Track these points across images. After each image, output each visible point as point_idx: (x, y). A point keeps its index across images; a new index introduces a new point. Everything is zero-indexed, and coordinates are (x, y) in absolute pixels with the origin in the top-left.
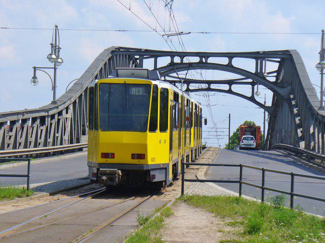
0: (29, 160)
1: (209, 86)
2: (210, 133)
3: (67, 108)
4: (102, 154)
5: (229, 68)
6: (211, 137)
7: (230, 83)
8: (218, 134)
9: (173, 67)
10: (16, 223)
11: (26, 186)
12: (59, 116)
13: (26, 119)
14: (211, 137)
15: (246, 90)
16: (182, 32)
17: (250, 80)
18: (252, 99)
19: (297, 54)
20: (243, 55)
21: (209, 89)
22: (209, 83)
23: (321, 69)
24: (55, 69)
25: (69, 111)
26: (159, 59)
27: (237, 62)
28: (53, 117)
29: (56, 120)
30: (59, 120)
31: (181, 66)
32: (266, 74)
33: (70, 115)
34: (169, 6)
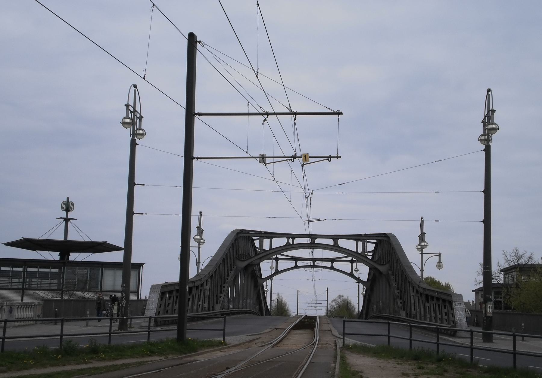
0: (225, 318)
1: (314, 263)
2: (310, 305)
3: (207, 281)
4: (472, 290)
5: (336, 247)
6: (311, 308)
7: (333, 260)
8: (318, 305)
9: (289, 247)
10: (241, 361)
11: (222, 339)
12: (201, 287)
13: (165, 292)
14: (311, 308)
15: (346, 267)
16: (320, 219)
17: (350, 258)
18: (351, 275)
19: (394, 237)
20: (347, 237)
21: (314, 266)
22: (314, 260)
23: (420, 250)
24: (199, 247)
25: (208, 283)
26: (274, 240)
27: (342, 243)
28: (197, 287)
29: (200, 291)
30: (201, 290)
31: (294, 246)
32: (366, 253)
33: (208, 287)
34: (309, 198)
